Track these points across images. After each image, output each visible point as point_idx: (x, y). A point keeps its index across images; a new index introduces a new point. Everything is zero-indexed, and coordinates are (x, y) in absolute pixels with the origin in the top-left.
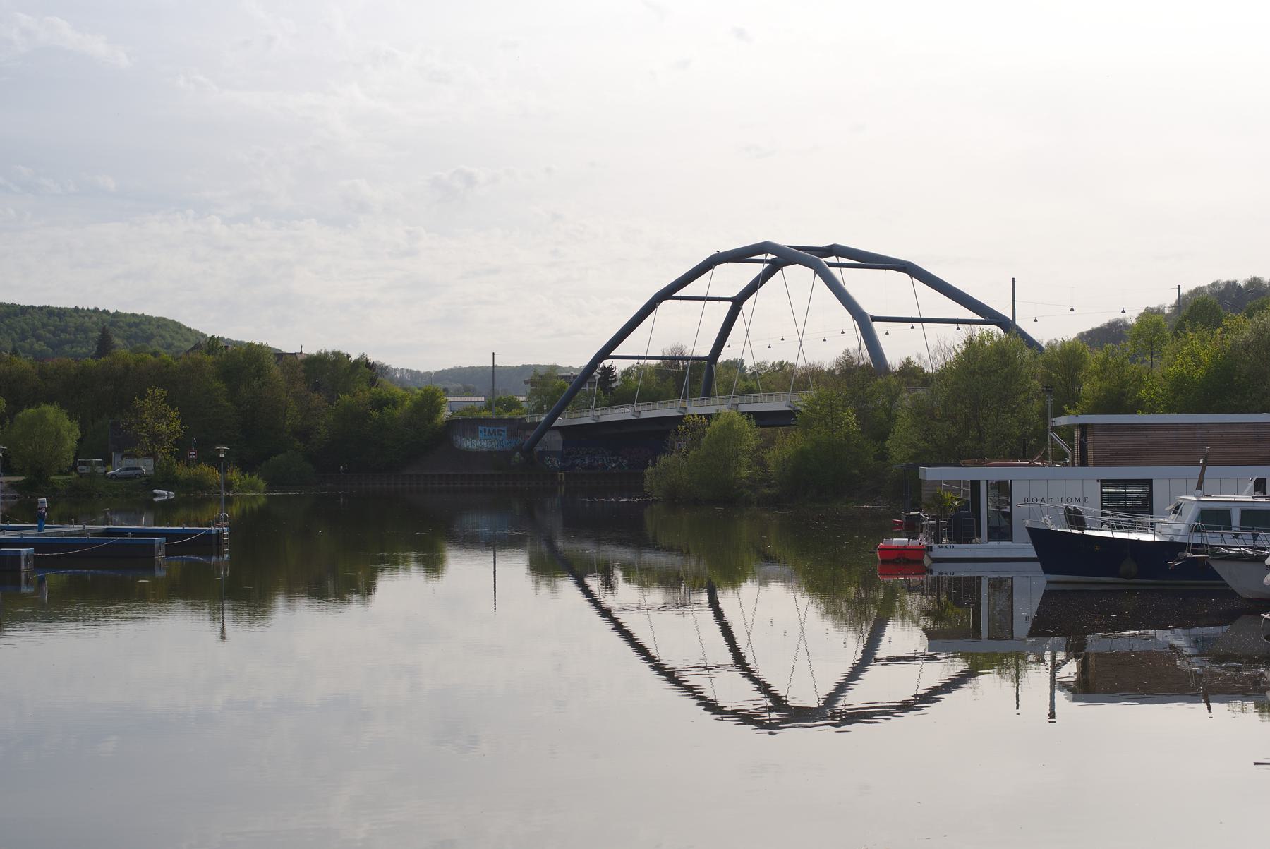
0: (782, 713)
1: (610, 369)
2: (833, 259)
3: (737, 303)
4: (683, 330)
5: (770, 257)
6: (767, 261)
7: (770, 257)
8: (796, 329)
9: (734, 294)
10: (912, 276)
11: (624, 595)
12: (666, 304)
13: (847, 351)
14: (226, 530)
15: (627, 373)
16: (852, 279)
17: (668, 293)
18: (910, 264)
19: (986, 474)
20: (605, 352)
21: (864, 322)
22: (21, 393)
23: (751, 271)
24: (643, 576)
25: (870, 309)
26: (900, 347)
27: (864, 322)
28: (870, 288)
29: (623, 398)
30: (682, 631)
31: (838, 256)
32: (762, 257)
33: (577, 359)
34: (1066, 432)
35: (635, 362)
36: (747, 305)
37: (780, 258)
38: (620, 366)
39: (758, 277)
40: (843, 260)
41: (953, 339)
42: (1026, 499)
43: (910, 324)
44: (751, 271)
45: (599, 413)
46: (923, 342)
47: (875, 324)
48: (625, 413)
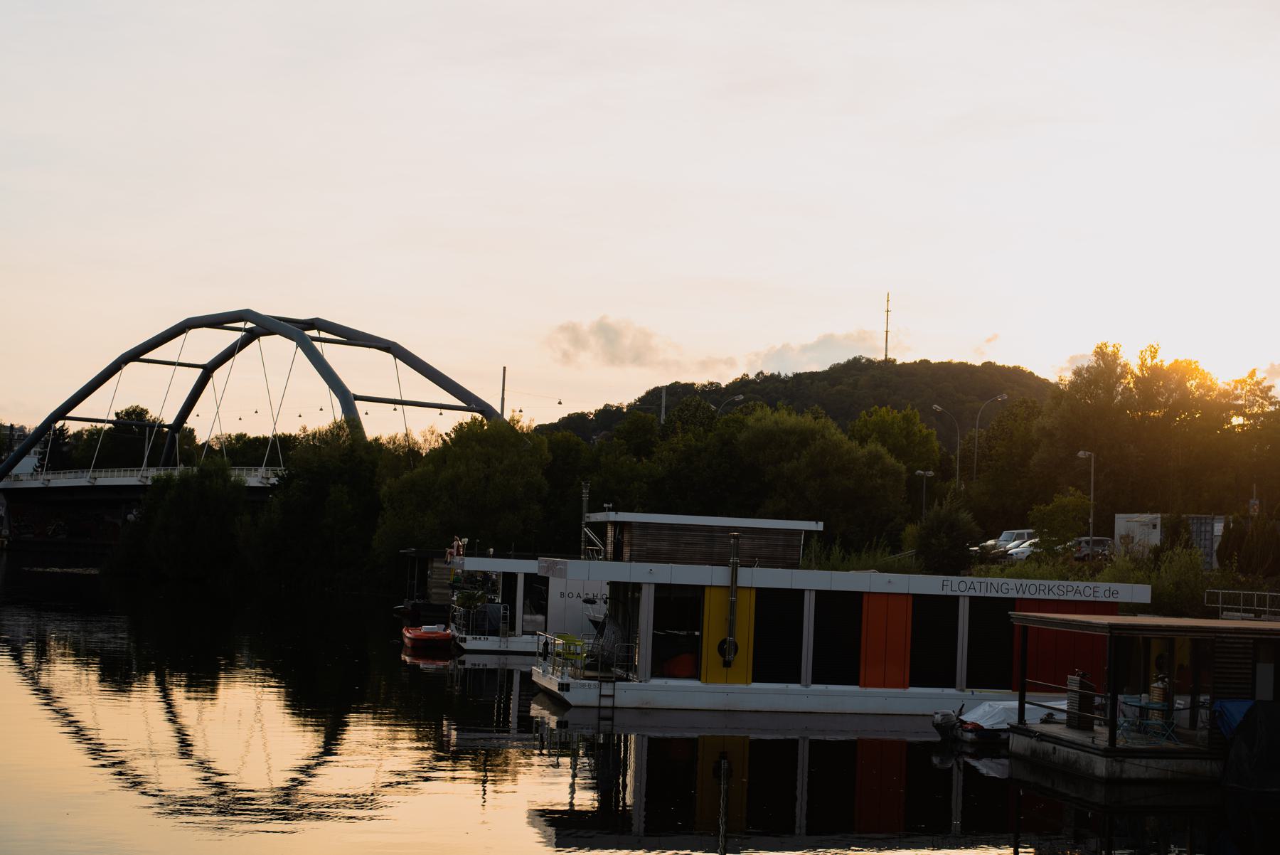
0: (228, 803)
1: (62, 430)
2: (314, 333)
3: (208, 371)
4: (154, 392)
5: (250, 325)
6: (246, 330)
7: (250, 325)
8: (268, 399)
9: (205, 360)
10: (396, 356)
11: (64, 674)
12: (132, 366)
13: (304, 429)
14: (1095, 727)
15: (78, 435)
16: (334, 354)
17: (135, 355)
18: (188, 320)
19: (522, 567)
20: (62, 413)
21: (347, 400)
22: (1275, 614)
23: (228, 338)
24: (82, 654)
25: (354, 389)
26: (379, 425)
27: (347, 400)
28: (361, 369)
29: (79, 464)
30: (134, 719)
31: (319, 330)
32: (241, 325)
33: (31, 421)
34: (600, 528)
35: (87, 425)
36: (219, 374)
37: (261, 327)
38: (73, 427)
39: (235, 343)
40: (324, 335)
41: (448, 423)
42: (562, 594)
43: (438, 411)
44: (228, 338)
45: (49, 477)
46: (410, 421)
47: (358, 403)
48: (80, 480)
